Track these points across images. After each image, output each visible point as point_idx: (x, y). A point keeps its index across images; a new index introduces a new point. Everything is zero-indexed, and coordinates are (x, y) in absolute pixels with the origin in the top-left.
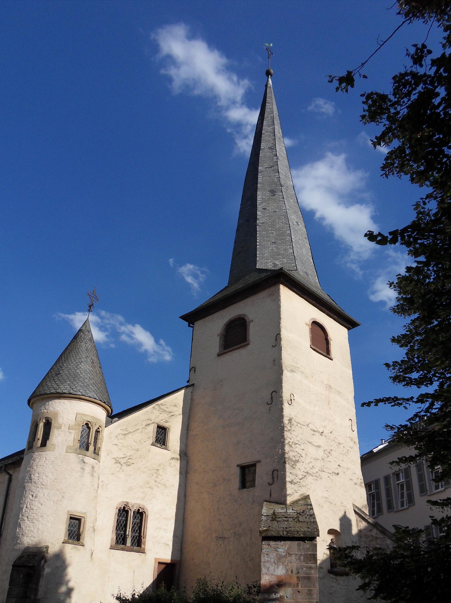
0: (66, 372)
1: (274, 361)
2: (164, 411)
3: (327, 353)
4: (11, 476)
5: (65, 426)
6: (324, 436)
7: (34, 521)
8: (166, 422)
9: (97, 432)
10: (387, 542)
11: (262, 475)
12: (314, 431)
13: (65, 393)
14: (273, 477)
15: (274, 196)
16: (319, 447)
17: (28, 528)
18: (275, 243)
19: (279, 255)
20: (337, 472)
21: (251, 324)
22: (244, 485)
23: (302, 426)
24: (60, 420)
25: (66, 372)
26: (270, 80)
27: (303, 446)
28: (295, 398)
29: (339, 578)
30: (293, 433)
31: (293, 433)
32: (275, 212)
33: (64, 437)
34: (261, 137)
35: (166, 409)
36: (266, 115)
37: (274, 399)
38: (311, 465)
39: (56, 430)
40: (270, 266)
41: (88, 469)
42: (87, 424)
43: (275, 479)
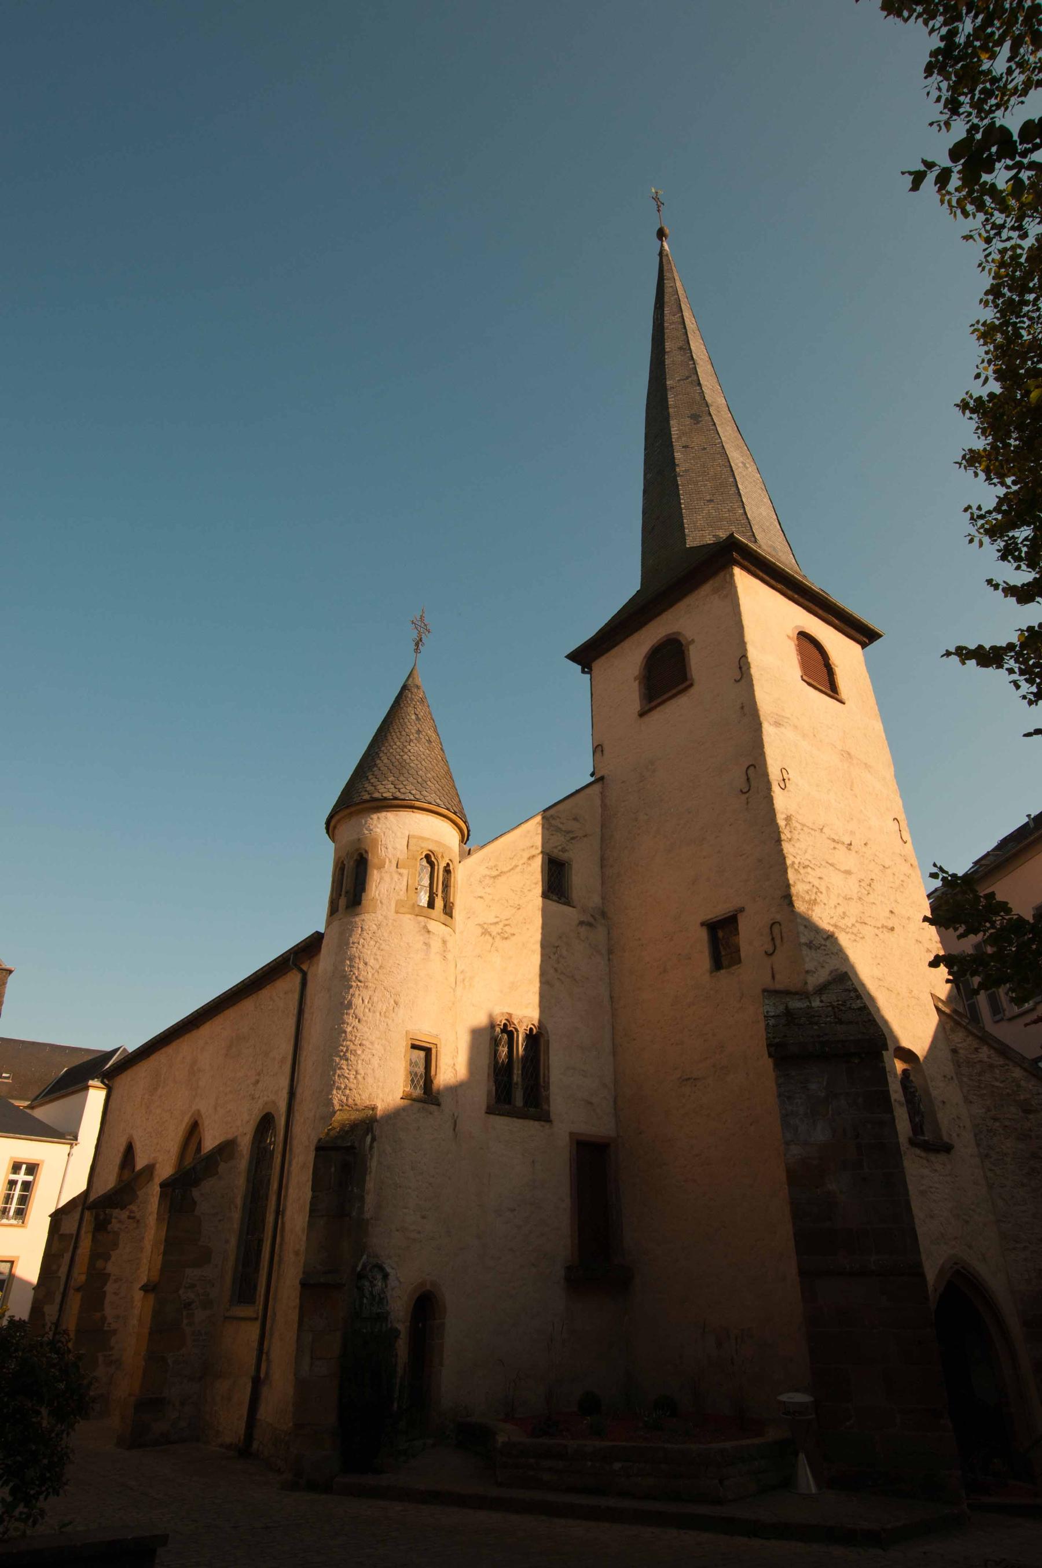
0: (386, 761)
1: (742, 708)
2: (558, 830)
3: (831, 689)
4: (304, 975)
5: (390, 862)
6: (853, 852)
7: (348, 1055)
8: (564, 850)
9: (447, 871)
10: (1014, 1075)
11: (750, 937)
12: (834, 841)
13: (385, 799)
14: (773, 939)
15: (698, 423)
16: (848, 872)
17: (338, 1072)
18: (711, 501)
19: (721, 520)
20: (891, 925)
21: (691, 647)
22: (718, 963)
23: (813, 832)
24: (382, 852)
25: (386, 761)
26: (665, 244)
27: (819, 872)
28: (790, 776)
29: (932, 1157)
30: (797, 845)
31: (797, 845)
32: (705, 449)
33: (389, 886)
34: (663, 334)
35: (561, 826)
36: (666, 299)
37: (753, 781)
38: (840, 910)
39: (375, 872)
40: (709, 540)
41: (436, 945)
42: (427, 857)
43: (778, 942)
